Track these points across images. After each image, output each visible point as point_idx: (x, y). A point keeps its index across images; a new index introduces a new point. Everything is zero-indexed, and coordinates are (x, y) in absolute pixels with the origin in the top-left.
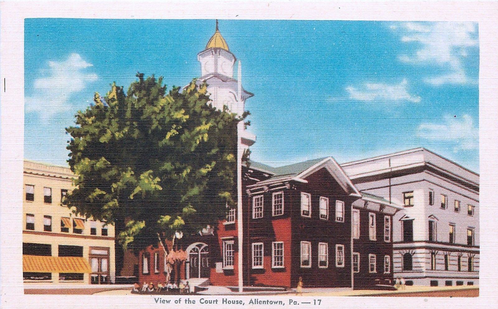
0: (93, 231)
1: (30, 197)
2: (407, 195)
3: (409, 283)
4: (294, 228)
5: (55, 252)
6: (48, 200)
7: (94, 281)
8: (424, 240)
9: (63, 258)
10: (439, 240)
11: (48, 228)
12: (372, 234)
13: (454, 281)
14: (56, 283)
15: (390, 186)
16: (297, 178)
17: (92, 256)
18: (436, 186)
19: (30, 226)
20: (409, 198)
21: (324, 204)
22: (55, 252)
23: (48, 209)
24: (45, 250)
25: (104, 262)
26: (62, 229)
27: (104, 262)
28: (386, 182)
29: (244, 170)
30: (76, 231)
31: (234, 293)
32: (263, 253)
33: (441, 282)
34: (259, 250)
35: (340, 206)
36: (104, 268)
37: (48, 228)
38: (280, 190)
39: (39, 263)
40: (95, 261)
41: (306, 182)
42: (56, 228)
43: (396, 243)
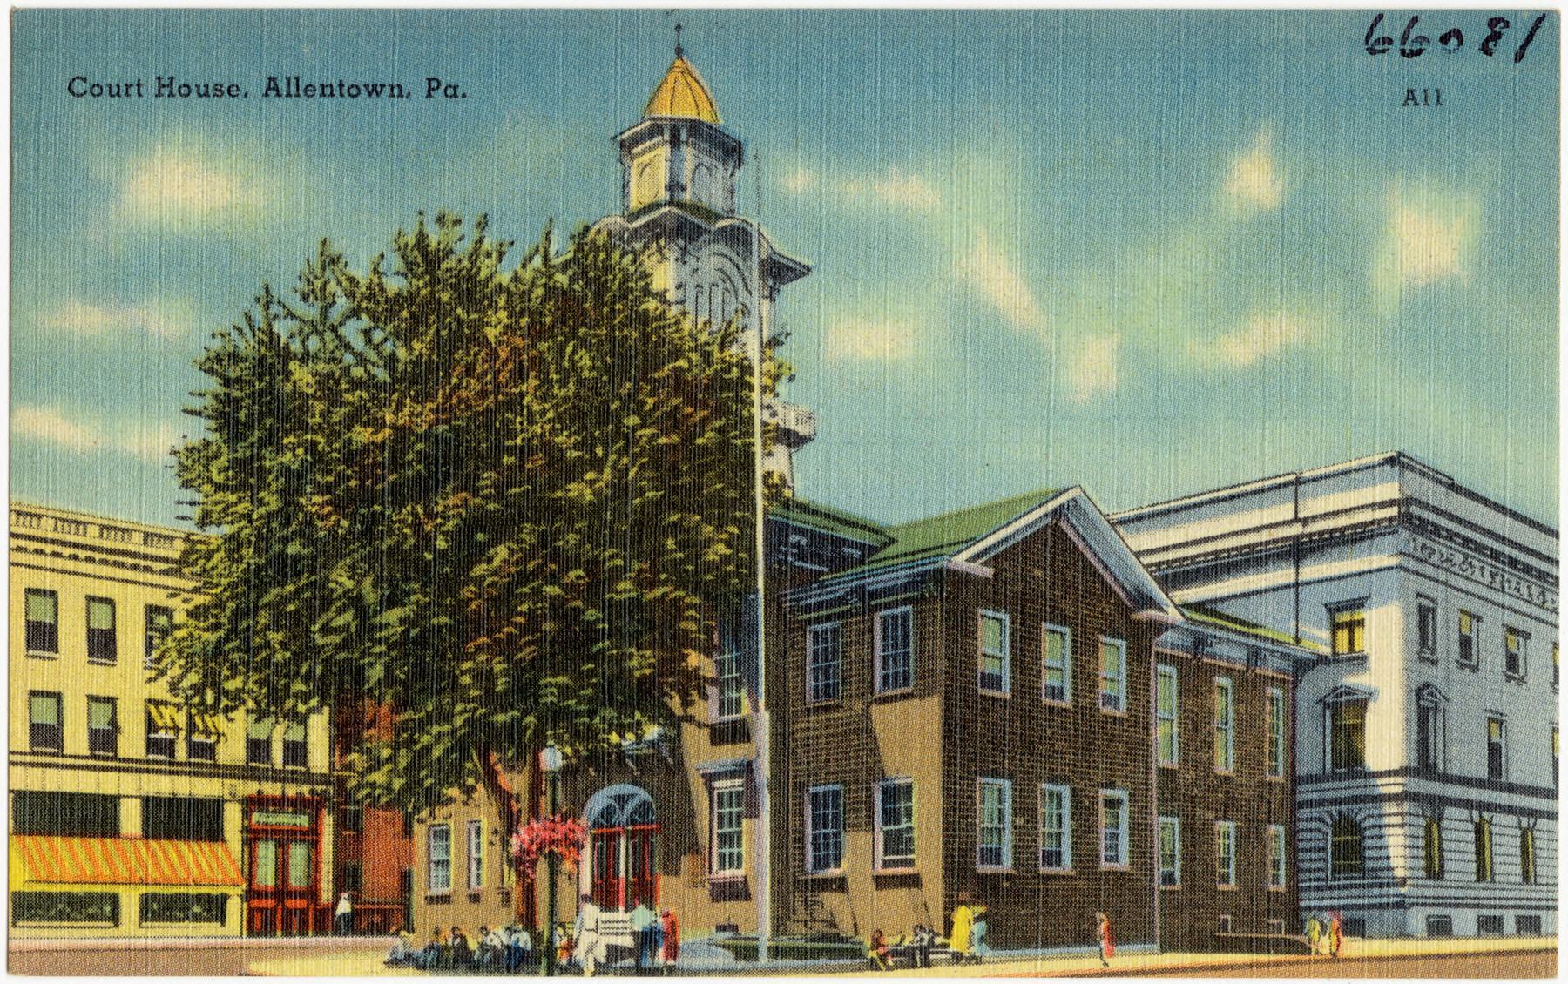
0: (258, 749)
1: (42, 637)
2: (1345, 617)
3: (1355, 927)
4: (953, 730)
5: (131, 818)
6: (103, 645)
7: (260, 923)
8: (1395, 766)
9: (153, 844)
10: (1454, 770)
11: (104, 740)
12: (1224, 762)
13: (1509, 918)
14: (131, 930)
15: (1297, 585)
16: (960, 561)
17: (252, 837)
18: (1412, 577)
19: (46, 736)
20: (1352, 626)
21: (1055, 648)
22: (131, 818)
23: (102, 679)
24: (94, 818)
25: (298, 853)
26: (148, 741)
27: (298, 853)
28: (1282, 574)
29: (777, 531)
30: (196, 749)
31: (742, 964)
32: (912, 655)
33: (1465, 920)
34: (891, 671)
35: (1113, 659)
36: (297, 877)
37: (104, 740)
38: (905, 602)
39: (73, 862)
40: (266, 852)
41: (988, 572)
42: (132, 743)
43: (1309, 779)
